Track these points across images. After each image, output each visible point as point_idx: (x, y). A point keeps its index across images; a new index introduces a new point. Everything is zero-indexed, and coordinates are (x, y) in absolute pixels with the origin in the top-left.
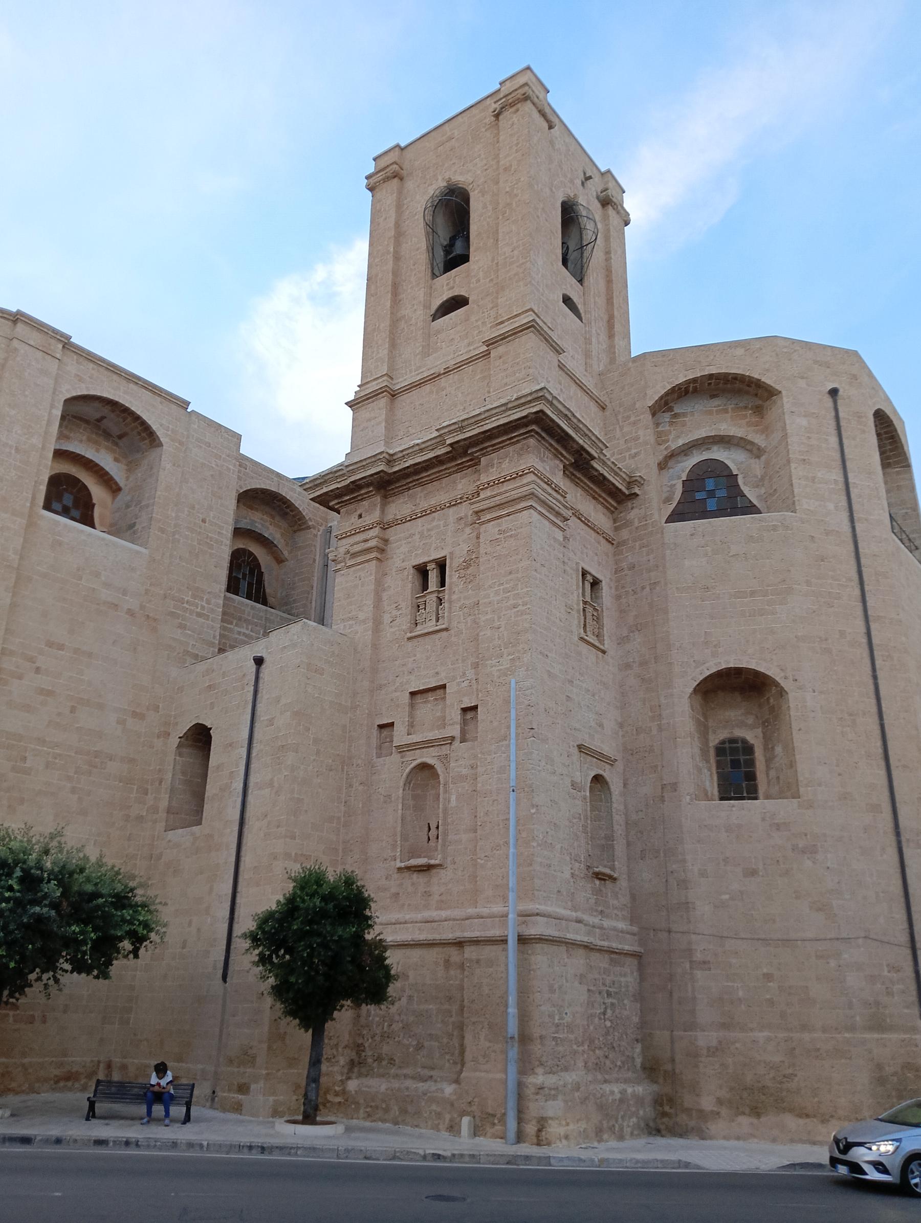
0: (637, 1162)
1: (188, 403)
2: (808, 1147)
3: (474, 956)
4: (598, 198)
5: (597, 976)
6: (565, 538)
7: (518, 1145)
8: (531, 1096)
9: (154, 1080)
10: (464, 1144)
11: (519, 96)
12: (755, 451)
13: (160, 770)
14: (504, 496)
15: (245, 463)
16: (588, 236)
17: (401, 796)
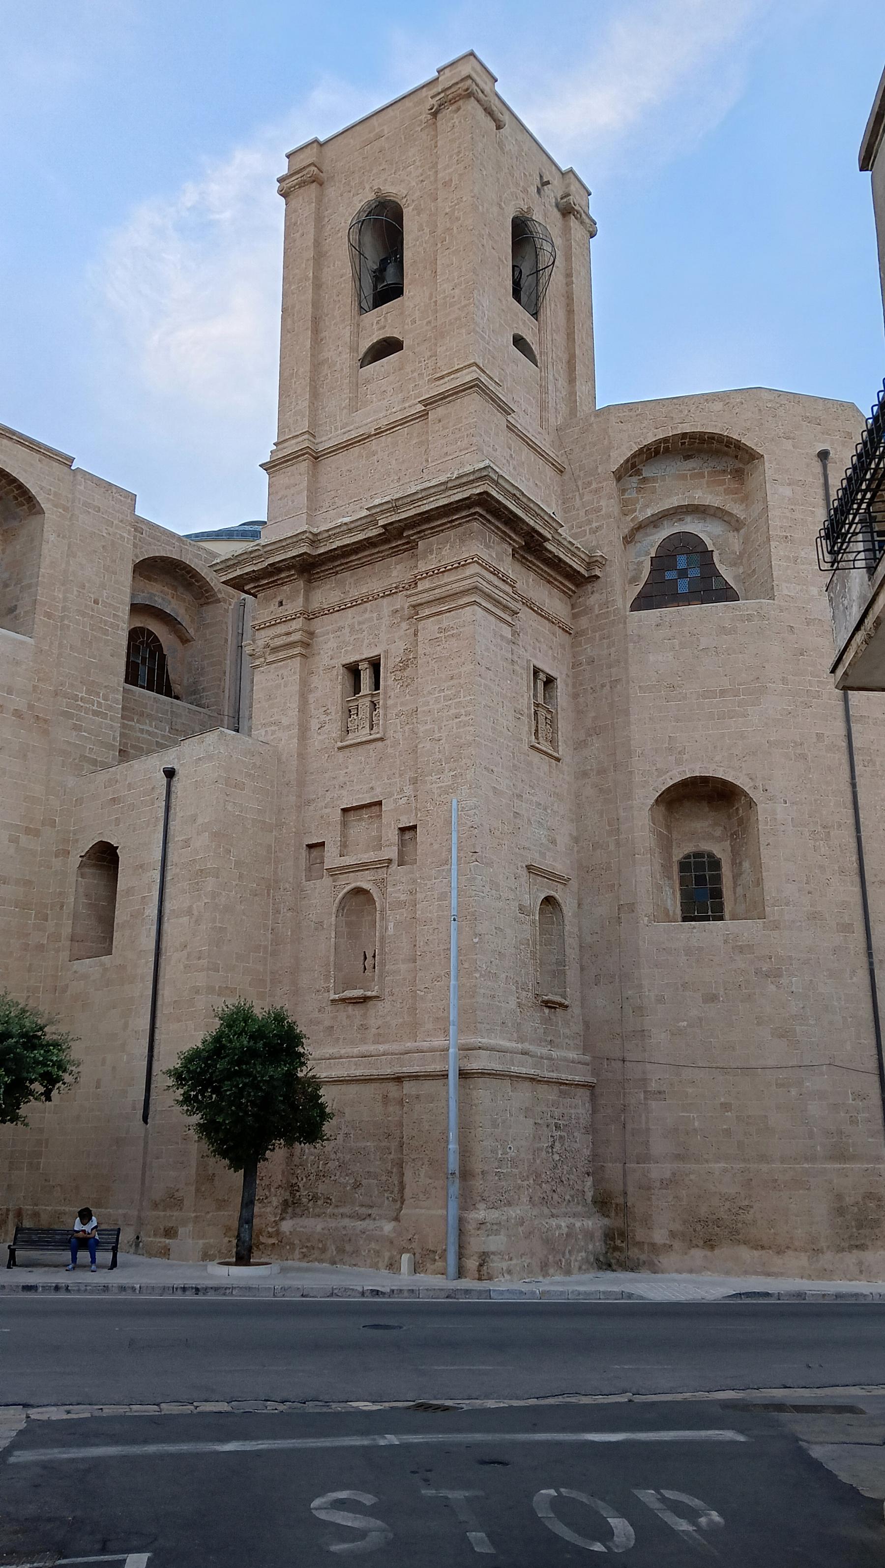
0: (579, 1293)
1: (72, 460)
2: (762, 1279)
3: (414, 1092)
4: (557, 205)
5: (545, 1109)
6: (515, 633)
7: (459, 1280)
8: (473, 1231)
9: (78, 1226)
10: (405, 1279)
11: (460, 91)
12: (734, 524)
13: (60, 893)
14: (444, 589)
15: (140, 526)
16: (545, 259)
17: (334, 923)
